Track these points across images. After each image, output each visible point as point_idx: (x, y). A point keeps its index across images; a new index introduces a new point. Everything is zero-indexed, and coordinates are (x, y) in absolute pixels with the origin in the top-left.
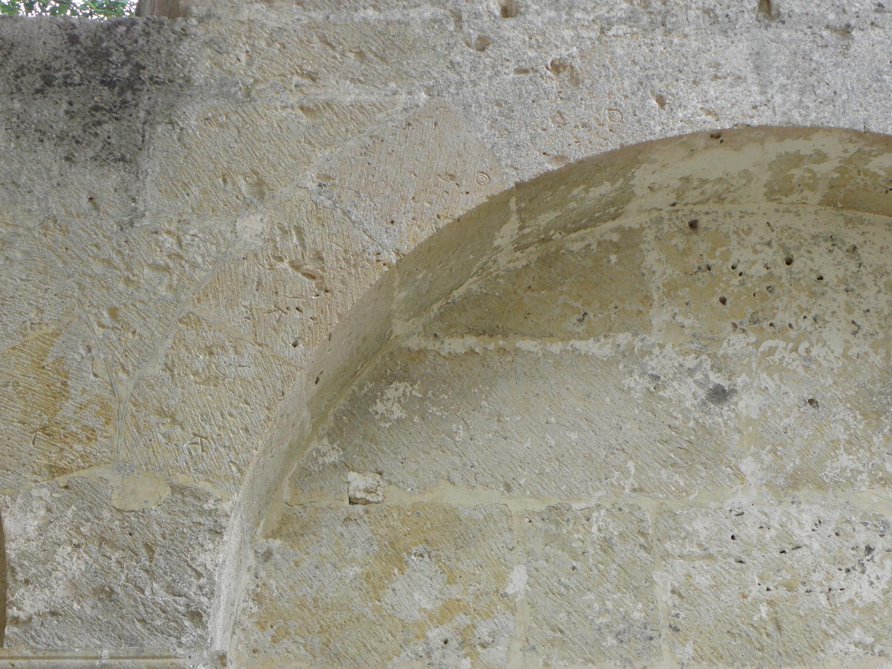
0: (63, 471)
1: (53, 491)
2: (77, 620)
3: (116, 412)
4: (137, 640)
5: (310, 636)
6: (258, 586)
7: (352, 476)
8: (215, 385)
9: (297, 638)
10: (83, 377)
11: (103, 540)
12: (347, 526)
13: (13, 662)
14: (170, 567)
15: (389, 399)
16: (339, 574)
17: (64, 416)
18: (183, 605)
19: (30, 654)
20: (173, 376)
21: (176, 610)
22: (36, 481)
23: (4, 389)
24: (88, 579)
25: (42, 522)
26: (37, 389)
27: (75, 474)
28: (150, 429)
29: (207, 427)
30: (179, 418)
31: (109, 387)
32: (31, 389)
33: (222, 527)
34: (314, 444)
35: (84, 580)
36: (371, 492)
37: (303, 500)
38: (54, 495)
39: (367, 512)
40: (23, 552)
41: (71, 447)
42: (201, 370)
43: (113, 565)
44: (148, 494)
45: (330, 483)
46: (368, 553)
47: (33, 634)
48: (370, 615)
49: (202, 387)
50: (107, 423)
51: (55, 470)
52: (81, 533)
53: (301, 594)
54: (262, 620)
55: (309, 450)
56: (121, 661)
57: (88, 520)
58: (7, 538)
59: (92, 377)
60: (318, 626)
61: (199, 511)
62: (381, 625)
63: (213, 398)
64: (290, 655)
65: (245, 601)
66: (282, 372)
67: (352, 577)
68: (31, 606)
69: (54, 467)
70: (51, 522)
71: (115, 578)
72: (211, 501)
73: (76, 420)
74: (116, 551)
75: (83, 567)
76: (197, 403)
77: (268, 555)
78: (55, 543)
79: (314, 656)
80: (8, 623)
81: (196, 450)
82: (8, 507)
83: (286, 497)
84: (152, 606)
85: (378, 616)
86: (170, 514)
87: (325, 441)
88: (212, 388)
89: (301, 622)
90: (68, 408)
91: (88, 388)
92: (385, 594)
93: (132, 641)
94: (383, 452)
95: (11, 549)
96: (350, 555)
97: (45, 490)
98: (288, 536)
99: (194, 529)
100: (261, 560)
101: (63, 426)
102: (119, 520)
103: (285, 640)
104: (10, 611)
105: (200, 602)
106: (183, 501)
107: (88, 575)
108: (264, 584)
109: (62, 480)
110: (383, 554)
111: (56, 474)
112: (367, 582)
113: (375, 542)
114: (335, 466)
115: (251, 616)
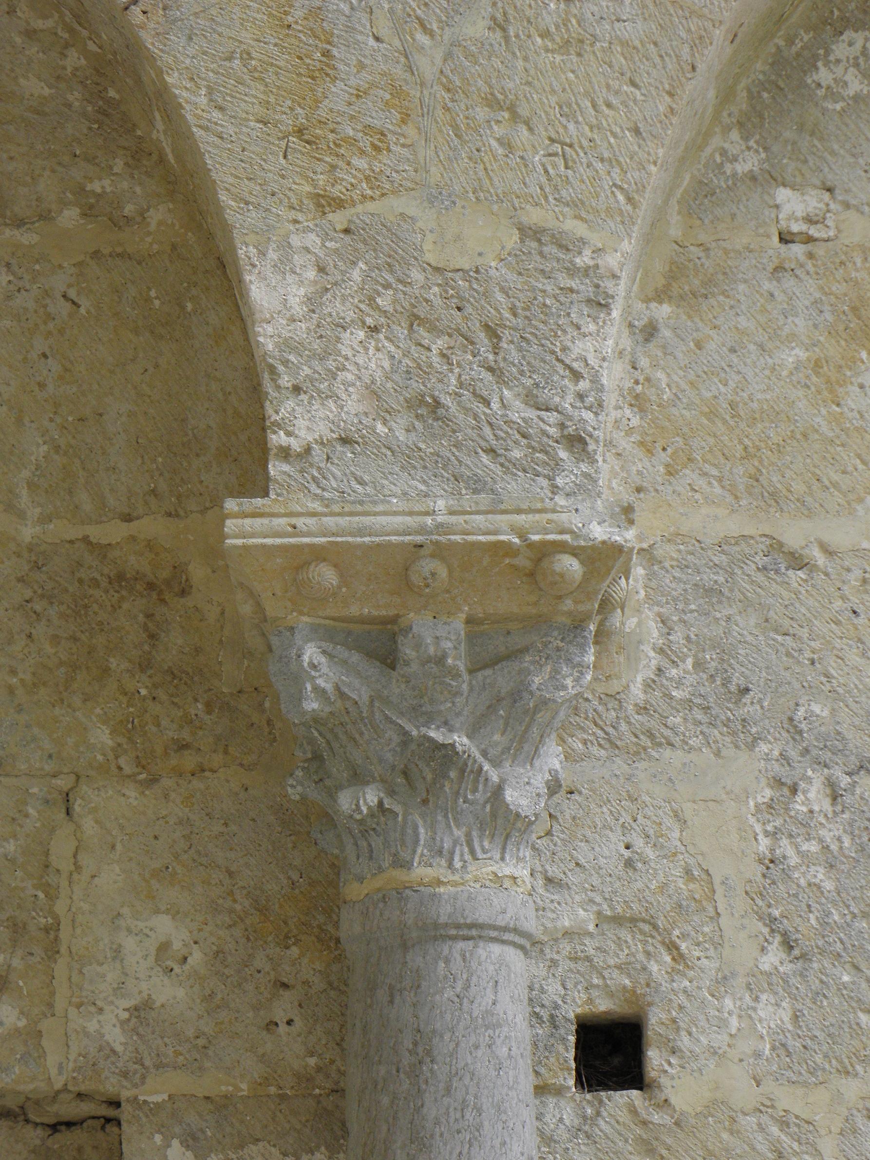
0: (339, 204)
1: (326, 237)
2: (384, 450)
3: (417, 101)
4: (486, 483)
5: (729, 465)
6: (637, 382)
7: (783, 194)
8: (579, 55)
9: (707, 468)
10: (357, 42)
11: (414, 319)
12: (778, 280)
13: (294, 521)
14: (528, 363)
15: (838, 61)
16: (770, 361)
17: (331, 110)
18: (555, 425)
19: (320, 509)
20: (507, 38)
21: (544, 433)
22: (296, 221)
23: (227, 64)
24: (396, 383)
25: (312, 289)
26: (282, 64)
27: (359, 208)
28: (476, 131)
29: (571, 126)
30: (524, 111)
31: (403, 59)
32: (272, 64)
33: (607, 296)
34: (717, 141)
35: (389, 385)
36: (816, 223)
37: (703, 237)
38: (328, 244)
39: (811, 256)
40: (286, 339)
41: (349, 164)
42: (553, 29)
43: (436, 360)
44: (482, 241)
45: (746, 207)
46: (815, 326)
47: (316, 474)
48: (825, 429)
49: (558, 58)
50: (404, 121)
51: (325, 203)
52: (378, 308)
53: (709, 395)
54: (649, 438)
55: (708, 150)
56: (467, 517)
57: (388, 286)
58: (257, 316)
59: (372, 42)
60: (740, 448)
61: (568, 269)
62: (843, 445)
63: (577, 77)
64: (697, 496)
65: (618, 407)
66: (689, 31)
67: (791, 366)
68: (308, 429)
69: (323, 196)
70: (327, 290)
71: (440, 381)
72: (587, 252)
73: (352, 117)
74: (439, 337)
75: (387, 364)
76: (551, 85)
77: (650, 331)
78: (337, 325)
79: (736, 497)
80: (271, 457)
81: (555, 166)
82: (254, 266)
83: (675, 232)
84: (505, 427)
85: (838, 431)
86: (520, 274)
87: (735, 135)
88: (574, 58)
89: (711, 441)
90: (337, 96)
91: (367, 62)
92: (847, 393)
93: (477, 485)
94: (833, 153)
95: (265, 336)
96: (787, 330)
97: (313, 236)
98: (682, 298)
99: (562, 299)
100: (640, 339)
101: (331, 126)
102: (439, 285)
103: (687, 472)
104: (274, 436)
105: (582, 420)
106: (541, 253)
107: (396, 377)
108: (648, 380)
109: (339, 219)
110: (841, 327)
111: (327, 209)
112: (817, 374)
113: (827, 308)
114: (754, 179)
115: (630, 431)
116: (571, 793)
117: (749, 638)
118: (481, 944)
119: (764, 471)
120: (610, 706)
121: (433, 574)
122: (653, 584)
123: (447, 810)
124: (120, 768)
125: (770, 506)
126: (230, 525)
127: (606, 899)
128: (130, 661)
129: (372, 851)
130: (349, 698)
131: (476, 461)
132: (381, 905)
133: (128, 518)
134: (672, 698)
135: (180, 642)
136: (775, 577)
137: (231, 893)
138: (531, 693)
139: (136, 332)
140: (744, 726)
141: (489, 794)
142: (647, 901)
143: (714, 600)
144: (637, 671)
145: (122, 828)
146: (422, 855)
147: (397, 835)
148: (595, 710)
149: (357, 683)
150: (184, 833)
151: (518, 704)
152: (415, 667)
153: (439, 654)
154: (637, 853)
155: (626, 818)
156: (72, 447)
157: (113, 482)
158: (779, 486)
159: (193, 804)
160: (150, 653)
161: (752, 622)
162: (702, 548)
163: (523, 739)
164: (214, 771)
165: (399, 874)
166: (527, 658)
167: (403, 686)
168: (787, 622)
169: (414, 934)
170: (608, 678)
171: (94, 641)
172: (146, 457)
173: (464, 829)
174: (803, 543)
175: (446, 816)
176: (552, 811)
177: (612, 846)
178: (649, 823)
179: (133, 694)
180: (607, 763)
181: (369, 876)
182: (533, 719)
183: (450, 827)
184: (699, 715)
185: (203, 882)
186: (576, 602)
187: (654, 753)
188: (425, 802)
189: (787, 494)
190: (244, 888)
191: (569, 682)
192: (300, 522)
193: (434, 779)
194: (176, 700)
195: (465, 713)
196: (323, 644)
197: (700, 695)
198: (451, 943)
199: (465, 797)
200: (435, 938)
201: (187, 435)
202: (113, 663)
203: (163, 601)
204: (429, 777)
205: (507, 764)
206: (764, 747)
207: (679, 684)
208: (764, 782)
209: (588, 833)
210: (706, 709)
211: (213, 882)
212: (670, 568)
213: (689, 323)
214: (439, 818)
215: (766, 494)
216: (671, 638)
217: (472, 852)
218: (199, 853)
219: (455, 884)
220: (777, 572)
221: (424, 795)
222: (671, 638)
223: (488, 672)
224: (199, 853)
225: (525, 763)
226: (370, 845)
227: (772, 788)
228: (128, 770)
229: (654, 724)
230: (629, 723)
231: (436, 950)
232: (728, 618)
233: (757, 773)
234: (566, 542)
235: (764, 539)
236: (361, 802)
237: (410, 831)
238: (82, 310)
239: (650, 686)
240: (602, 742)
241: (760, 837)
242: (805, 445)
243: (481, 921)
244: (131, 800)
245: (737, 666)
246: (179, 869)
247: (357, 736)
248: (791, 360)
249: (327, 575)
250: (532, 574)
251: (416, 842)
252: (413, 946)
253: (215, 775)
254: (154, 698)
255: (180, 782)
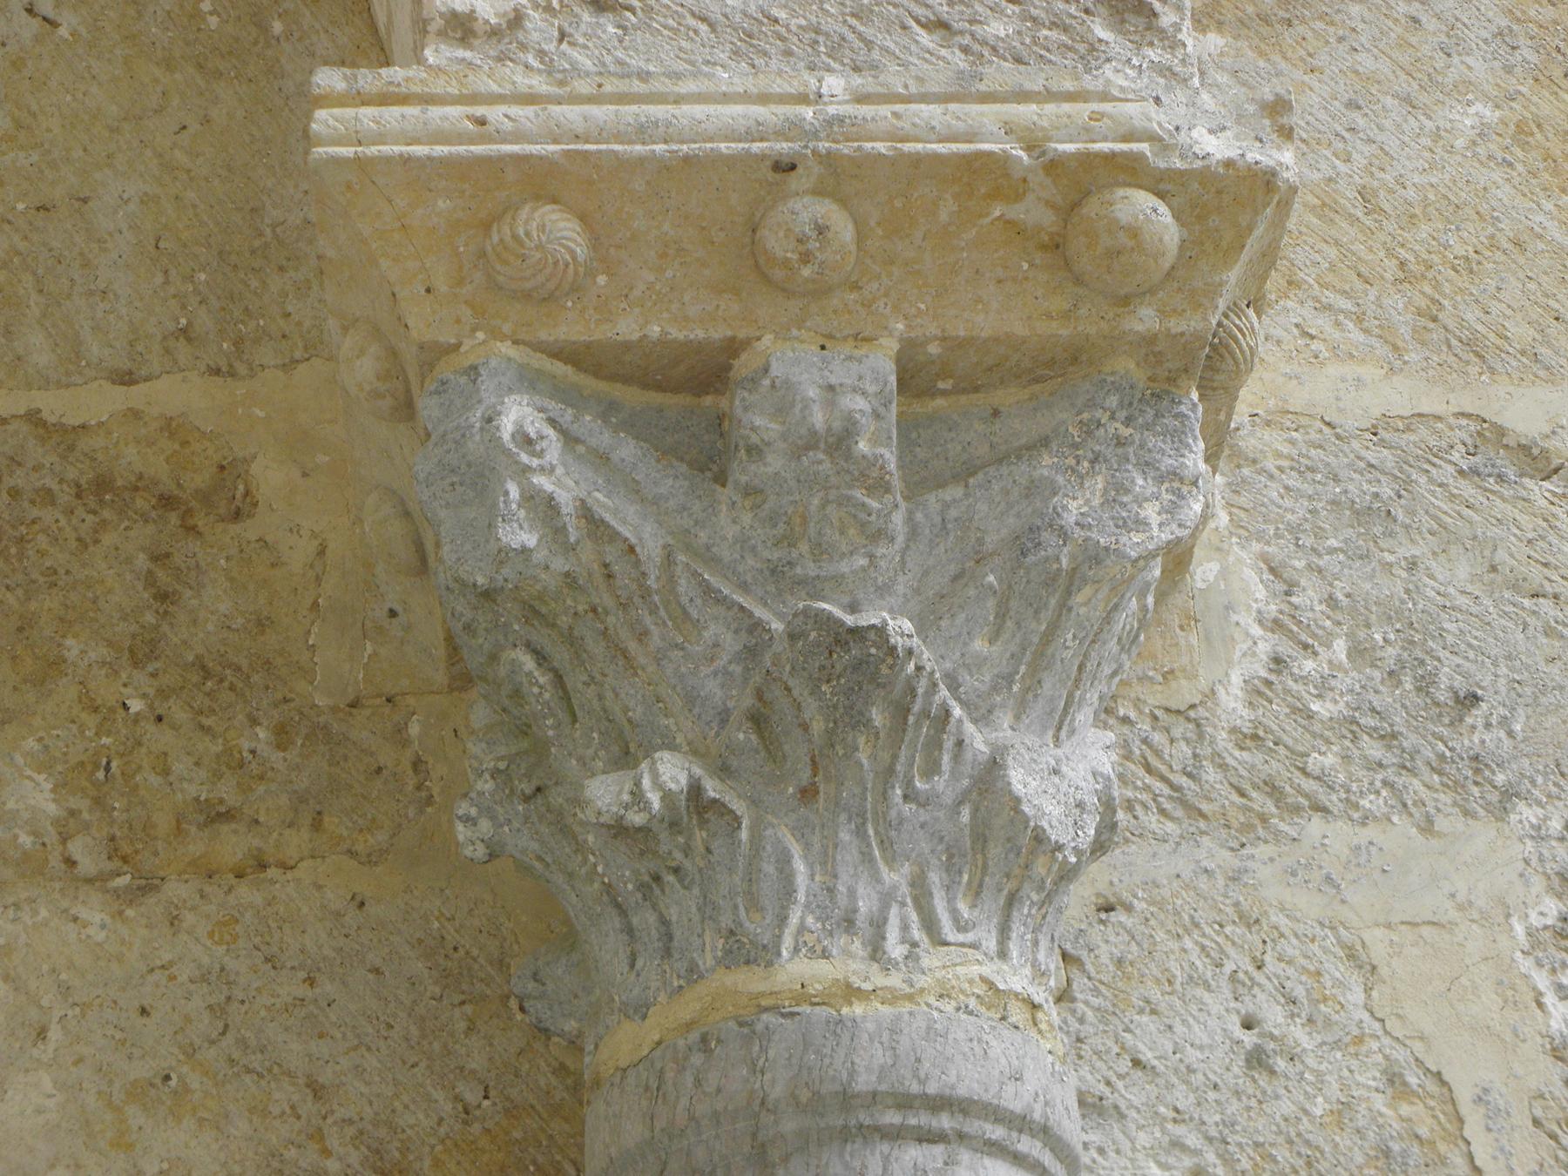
2: (692, 22)
9: (1330, 297)
13: (480, 111)
16: (1429, 124)
56: (898, 107)
60: (1391, 264)
79: (1396, 348)
89: (1333, 252)
96: (1452, 76)
103: (1290, 304)
112: (1524, 146)
113: (1522, 41)
116: (1109, 909)
117: (1462, 601)
118: (965, 1156)
119: (1446, 303)
120: (1177, 732)
121: (821, 230)
122: (1243, 501)
123: (862, 814)
124: (71, 862)
125: (1468, 363)
126: (324, 119)
127: (1210, 1140)
128: (110, 644)
129: (670, 937)
130: (614, 536)
131: (906, 41)
132: (697, 1059)
133: (126, 379)
134: (1310, 716)
135: (224, 607)
136: (1497, 488)
137: (318, 1136)
138: (1064, 534)
139: (168, 64)
140: (1477, 771)
141: (966, 782)
142: (1308, 1143)
143: (1378, 530)
144: (1230, 663)
145: (65, 990)
146: (802, 929)
147: (737, 879)
148: (1145, 741)
149: (632, 511)
150: (212, 1000)
151: (1031, 559)
152: (775, 463)
153: (837, 425)
154: (1272, 1037)
155: (1238, 961)
156: (19, 253)
157: (100, 314)
158: (1480, 327)
159: (235, 938)
160: (157, 627)
161: (1463, 571)
162: (1338, 437)
163: (1040, 658)
164: (286, 867)
165: (749, 981)
166: (1047, 460)
167: (747, 518)
168: (1536, 574)
169: (789, 1126)
170: (1168, 675)
171: (33, 606)
172: (173, 272)
173: (907, 868)
174: (1547, 429)
175: (860, 832)
176: (1068, 947)
177: (1213, 1023)
178: (1291, 971)
179: (112, 710)
180: (1184, 845)
181: (662, 998)
182: (1064, 607)
183: (871, 860)
184: (1375, 750)
185: (252, 1110)
186: (1162, 313)
187: (1283, 827)
188: (808, 794)
189: (1499, 342)
190: (351, 1122)
191: (1151, 512)
192: (495, 113)
193: (830, 733)
194: (207, 722)
195: (900, 589)
196: (552, 405)
197: (1373, 710)
198: (885, 1147)
199: (909, 783)
200: (846, 1135)
201: (261, 235)
202: (72, 647)
203: (192, 530)
204: (818, 726)
205: (1005, 719)
206: (1526, 813)
207: (1323, 688)
208: (1538, 884)
209: (1155, 994)
210: (1389, 738)
211: (276, 1111)
212: (1276, 473)
213: (1261, 64)
214: (845, 836)
215: (1454, 342)
216: (1294, 599)
217: (930, 925)
218: (243, 1043)
219: (893, 997)
220: (1501, 478)
221: (805, 776)
222: (1294, 599)
223: (954, 492)
224: (243, 1043)
225: (1044, 728)
226: (664, 922)
227: (1559, 896)
228: (88, 864)
229: (1276, 768)
230: (1224, 767)
231: (847, 1166)
232: (1412, 565)
233: (1521, 865)
234: (1139, 157)
235: (1464, 422)
236: (646, 782)
237: (769, 868)
238: (63, 31)
239: (1259, 693)
240: (1167, 806)
241: (1550, 999)
242: (1522, 261)
243: (962, 1091)
244: (91, 931)
245: (1442, 654)
246: (195, 1081)
247: (632, 646)
248: (1468, 122)
249: (557, 230)
250: (1056, 246)
251: (788, 892)
252: (786, 1159)
253: (289, 875)
254: (160, 719)
255: (208, 889)
